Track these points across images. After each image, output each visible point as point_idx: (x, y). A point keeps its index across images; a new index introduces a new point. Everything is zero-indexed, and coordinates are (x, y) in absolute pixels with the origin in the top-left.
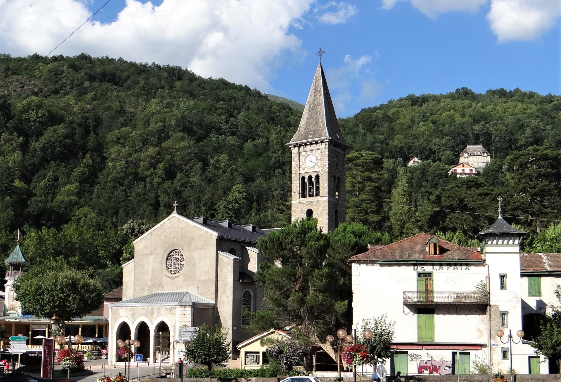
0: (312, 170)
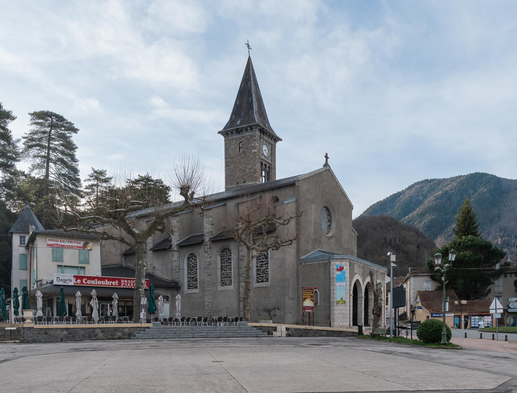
0: (265, 159)
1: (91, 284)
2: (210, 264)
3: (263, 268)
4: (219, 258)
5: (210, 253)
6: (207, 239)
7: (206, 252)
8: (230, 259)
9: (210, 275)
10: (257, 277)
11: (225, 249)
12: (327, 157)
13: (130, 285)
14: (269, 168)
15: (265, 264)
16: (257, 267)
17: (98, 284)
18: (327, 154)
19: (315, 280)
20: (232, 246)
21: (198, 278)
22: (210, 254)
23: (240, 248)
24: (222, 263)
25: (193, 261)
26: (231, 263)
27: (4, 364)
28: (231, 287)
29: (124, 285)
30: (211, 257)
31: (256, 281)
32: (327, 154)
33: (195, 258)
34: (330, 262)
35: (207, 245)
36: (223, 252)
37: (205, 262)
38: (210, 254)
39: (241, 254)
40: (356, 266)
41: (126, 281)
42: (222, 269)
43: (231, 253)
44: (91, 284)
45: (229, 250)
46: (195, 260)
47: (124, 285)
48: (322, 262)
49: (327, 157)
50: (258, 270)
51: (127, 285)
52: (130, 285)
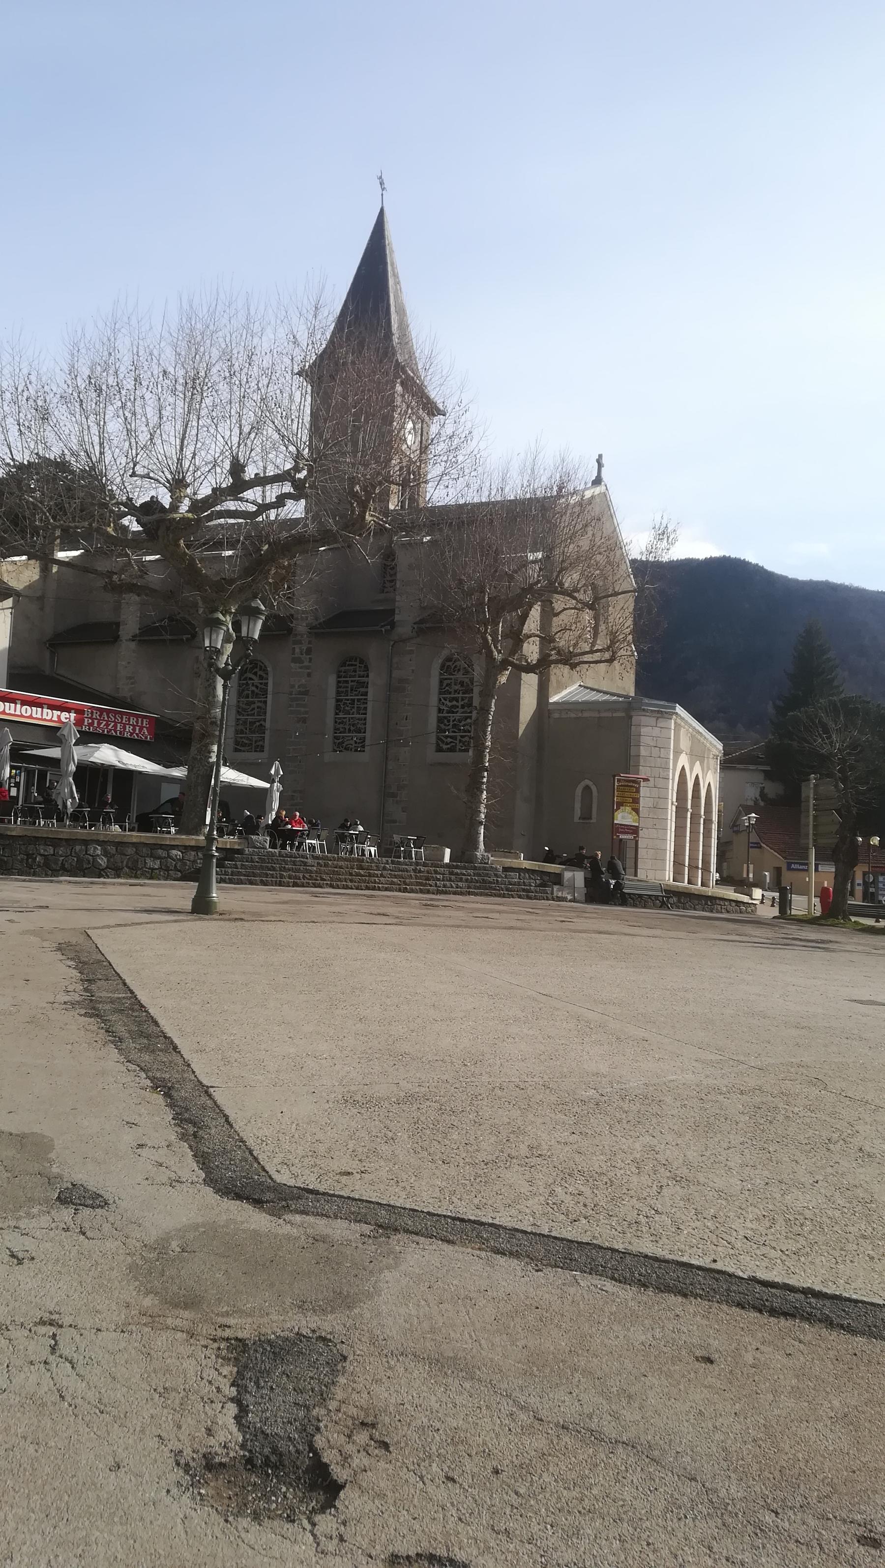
1: (31, 717)
2: (306, 693)
3: (458, 716)
4: (332, 680)
5: (306, 664)
6: (301, 628)
7: (295, 660)
8: (365, 685)
9: (304, 721)
10: (438, 738)
11: (351, 659)
12: (600, 465)
13: (107, 725)
14: (412, 480)
15: (463, 707)
16: (440, 711)
17: (22, 716)
18: (600, 456)
19: (591, 761)
20: (373, 651)
21: (268, 725)
22: (308, 668)
23: (395, 660)
24: (338, 693)
25: (256, 681)
26: (366, 694)
27: (860, 1282)
28: (364, 757)
29: (91, 724)
30: (309, 675)
31: (433, 747)
32: (600, 456)
33: (259, 673)
34: (631, 717)
35: (300, 642)
36: (344, 664)
37: (293, 686)
38: (308, 668)
39: (396, 674)
40: (682, 730)
41: (133, 721)
42: (338, 707)
43: (367, 669)
44: (31, 717)
45: (362, 662)
46: (261, 678)
47: (91, 724)
48: (609, 714)
49: (600, 465)
50: (440, 720)
51: (99, 724)
52: (107, 725)
